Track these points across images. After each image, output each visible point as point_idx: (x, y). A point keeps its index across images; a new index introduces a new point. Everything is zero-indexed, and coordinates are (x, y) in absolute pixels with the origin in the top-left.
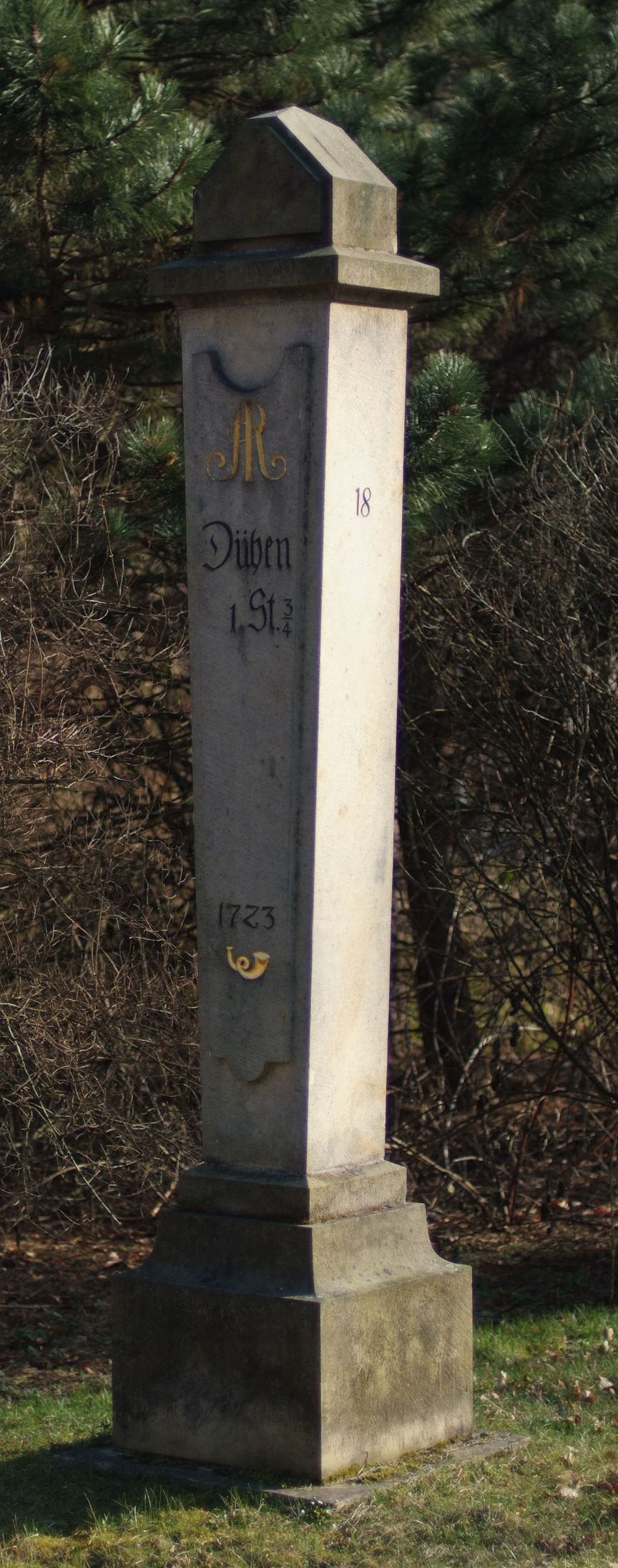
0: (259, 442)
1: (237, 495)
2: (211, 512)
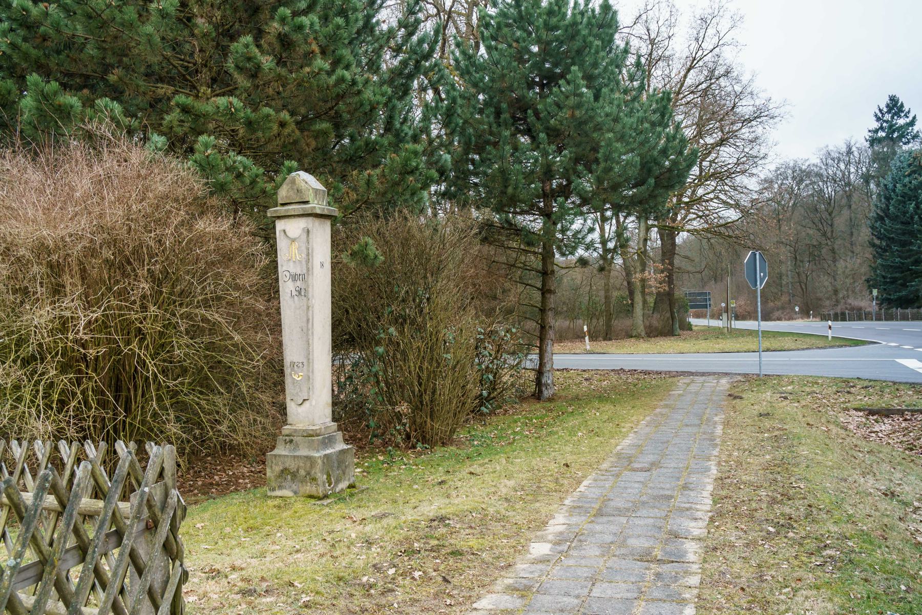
1: (291, 264)
2: (284, 268)
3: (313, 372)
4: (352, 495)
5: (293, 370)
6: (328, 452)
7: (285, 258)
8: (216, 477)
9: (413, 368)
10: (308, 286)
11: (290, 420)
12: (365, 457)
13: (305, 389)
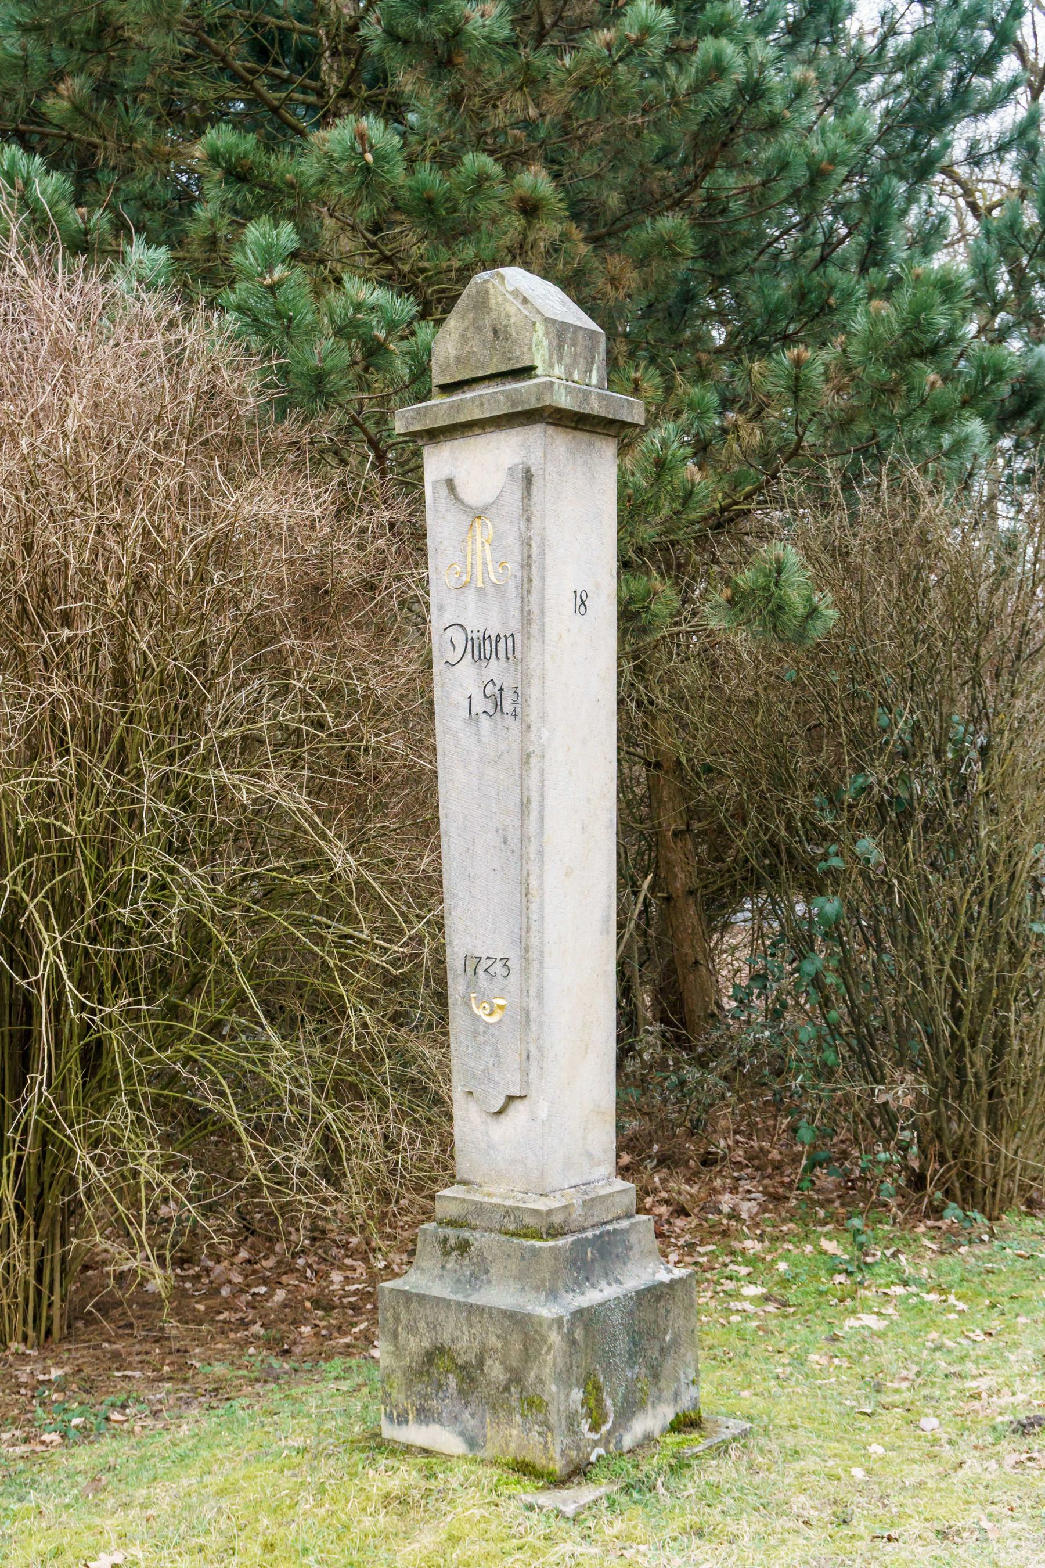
0: (488, 552)
1: (471, 597)
2: (449, 618)
3: (540, 991)
4: (679, 1466)
5: (472, 985)
6: (592, 1297)
7: (451, 580)
8: (336, 1277)
9: (931, 969)
10: (526, 677)
11: (463, 1166)
12: (783, 1238)
13: (512, 1060)
